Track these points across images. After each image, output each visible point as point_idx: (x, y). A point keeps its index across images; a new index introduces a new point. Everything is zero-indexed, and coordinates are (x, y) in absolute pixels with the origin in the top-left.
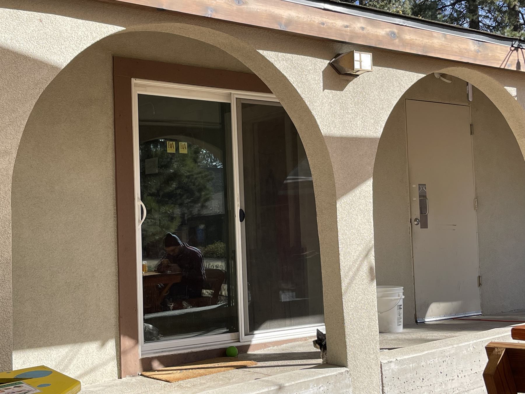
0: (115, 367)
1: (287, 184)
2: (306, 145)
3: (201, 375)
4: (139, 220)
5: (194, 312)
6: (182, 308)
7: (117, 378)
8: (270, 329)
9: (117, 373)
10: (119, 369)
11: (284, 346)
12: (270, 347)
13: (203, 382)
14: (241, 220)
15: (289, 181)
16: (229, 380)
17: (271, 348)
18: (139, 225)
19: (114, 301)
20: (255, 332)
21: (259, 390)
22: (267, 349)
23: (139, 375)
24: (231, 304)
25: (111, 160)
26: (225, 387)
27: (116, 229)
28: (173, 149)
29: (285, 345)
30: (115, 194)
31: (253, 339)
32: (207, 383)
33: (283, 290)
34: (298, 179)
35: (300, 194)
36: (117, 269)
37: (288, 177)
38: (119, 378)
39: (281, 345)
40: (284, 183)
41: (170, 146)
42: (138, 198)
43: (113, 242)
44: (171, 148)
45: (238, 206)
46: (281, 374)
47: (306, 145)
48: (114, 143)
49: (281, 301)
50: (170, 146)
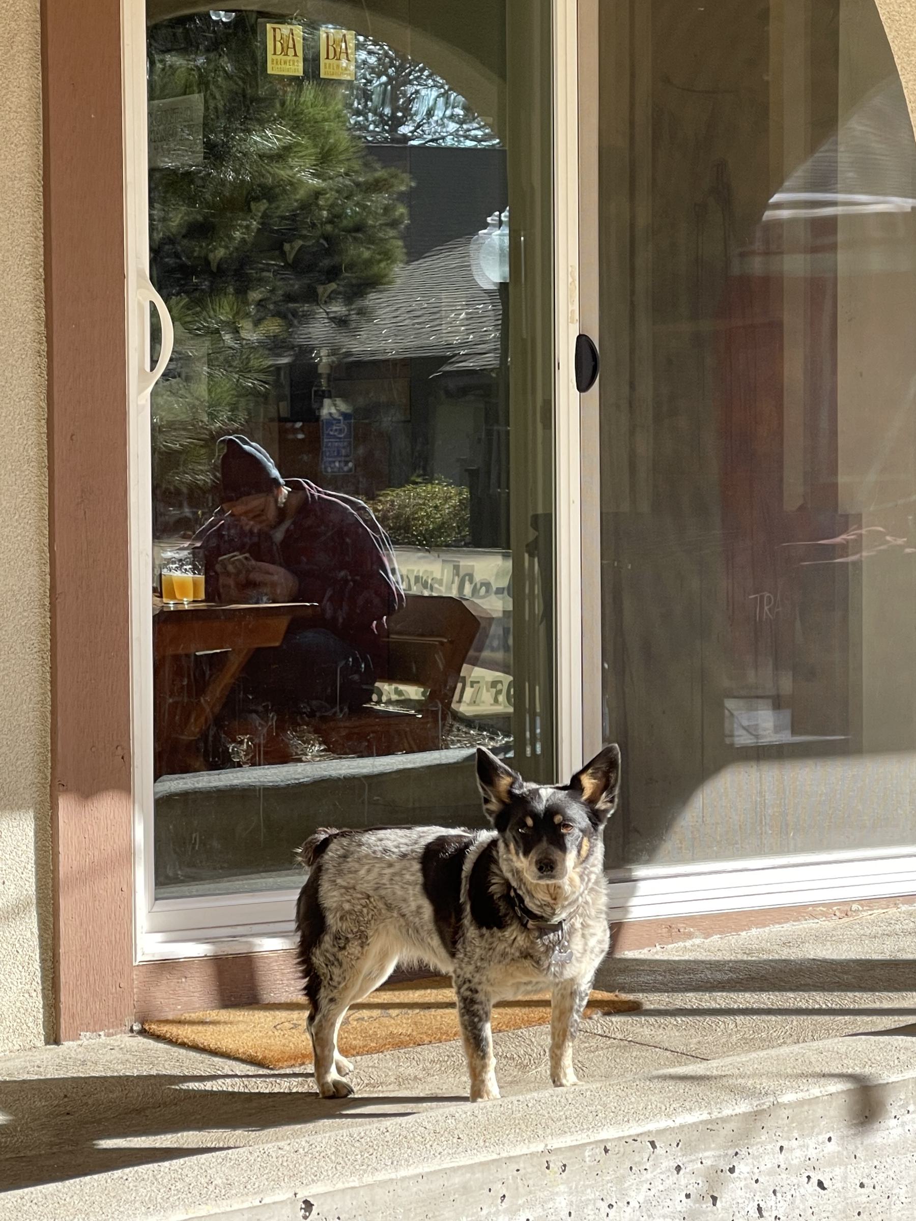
0: (34, 994)
1: (779, 224)
2: (908, 55)
3: (402, 1043)
4: (141, 369)
5: (369, 778)
6: (283, 757)
7: (40, 1042)
8: (693, 860)
9: (41, 1022)
10: (52, 1001)
11: (787, 928)
12: (690, 936)
13: (410, 1071)
14: (583, 385)
15: (785, 214)
16: (523, 1067)
17: (697, 941)
18: (141, 391)
19: (31, 715)
20: (640, 871)
21: (668, 1116)
22: (681, 944)
23: (132, 1030)
24: (528, 750)
25: (24, 100)
26: (521, 1098)
27: (44, 405)
28: (291, 56)
29: (754, 931)
30: (42, 251)
31: (634, 901)
32: (429, 1079)
33: (752, 697)
34: (834, 204)
35: (840, 274)
36: (48, 577)
37: (777, 198)
38: (47, 1043)
39: (738, 929)
40: (764, 218)
41: (278, 45)
42: (140, 273)
43: (29, 461)
44: (284, 52)
45: (569, 321)
46: (762, 1054)
47: (908, 55)
48: (38, 25)
49: (732, 745)
50: (278, 45)
